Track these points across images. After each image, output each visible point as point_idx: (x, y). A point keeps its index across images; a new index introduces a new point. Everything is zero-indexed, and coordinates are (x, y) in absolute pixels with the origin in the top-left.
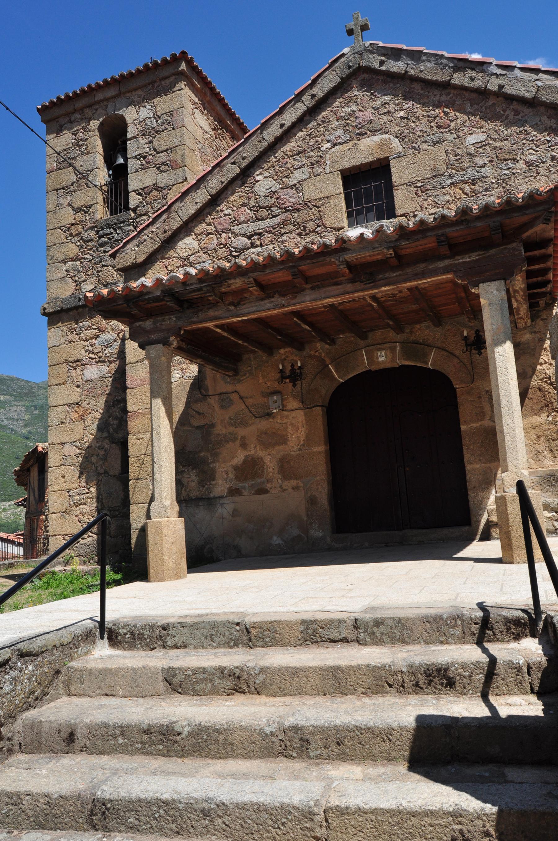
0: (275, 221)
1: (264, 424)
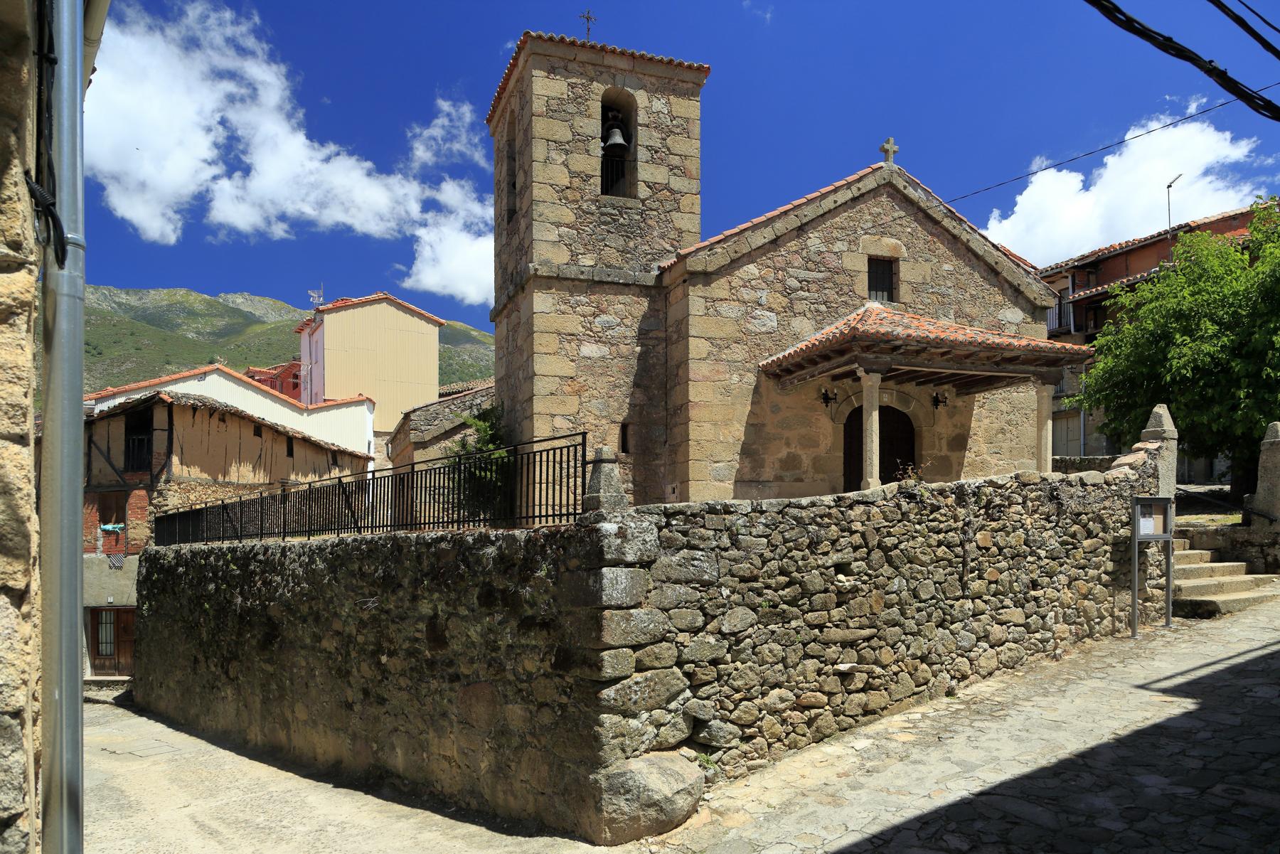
0: (821, 275)
1: (803, 431)
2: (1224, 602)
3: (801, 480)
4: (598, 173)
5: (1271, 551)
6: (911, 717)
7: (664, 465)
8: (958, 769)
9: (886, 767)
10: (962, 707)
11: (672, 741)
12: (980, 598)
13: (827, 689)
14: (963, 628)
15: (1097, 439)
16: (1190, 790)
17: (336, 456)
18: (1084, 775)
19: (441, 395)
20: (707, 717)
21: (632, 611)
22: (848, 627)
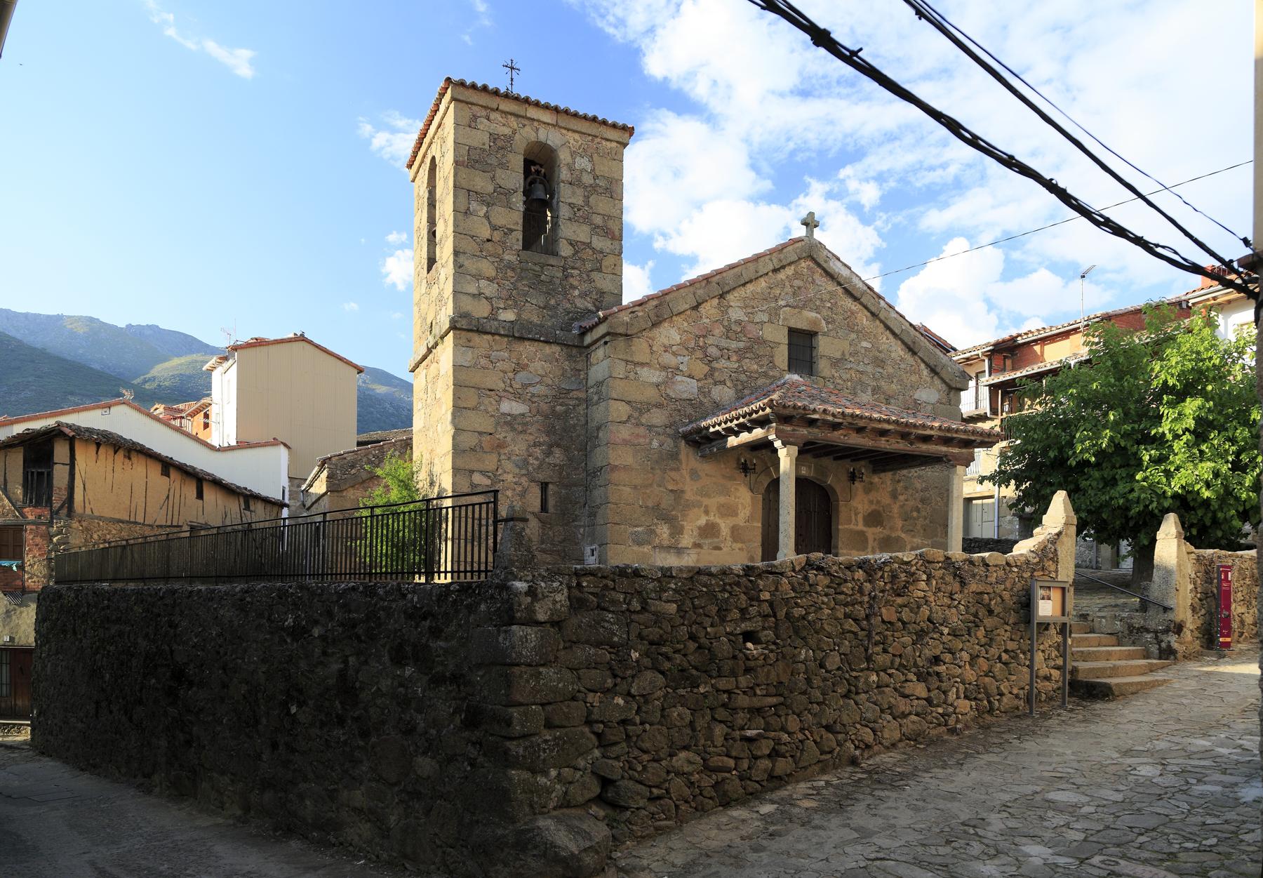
1: (722, 499)
2: (1117, 685)
3: (719, 548)
4: (520, 227)
5: (1164, 637)
6: (815, 784)
7: (584, 526)
8: (856, 835)
9: (788, 832)
10: (865, 776)
11: (581, 800)
12: (885, 671)
13: (734, 754)
14: (868, 700)
15: (1010, 522)
16: (1070, 860)
17: (248, 498)
18: (973, 843)
19: (359, 444)
20: (615, 777)
21: (541, 669)
22: (755, 694)
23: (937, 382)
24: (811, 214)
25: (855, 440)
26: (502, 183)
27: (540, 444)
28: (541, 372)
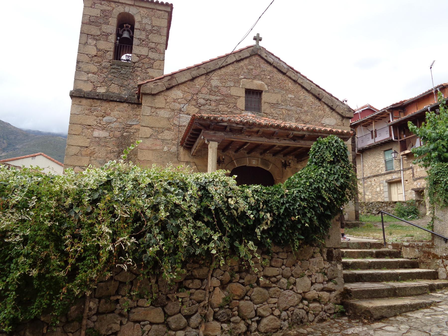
4: (112, 49)
23: (334, 114)
24: (258, 34)
25: (255, 140)
26: (104, 30)
27: (114, 152)
28: (117, 116)
